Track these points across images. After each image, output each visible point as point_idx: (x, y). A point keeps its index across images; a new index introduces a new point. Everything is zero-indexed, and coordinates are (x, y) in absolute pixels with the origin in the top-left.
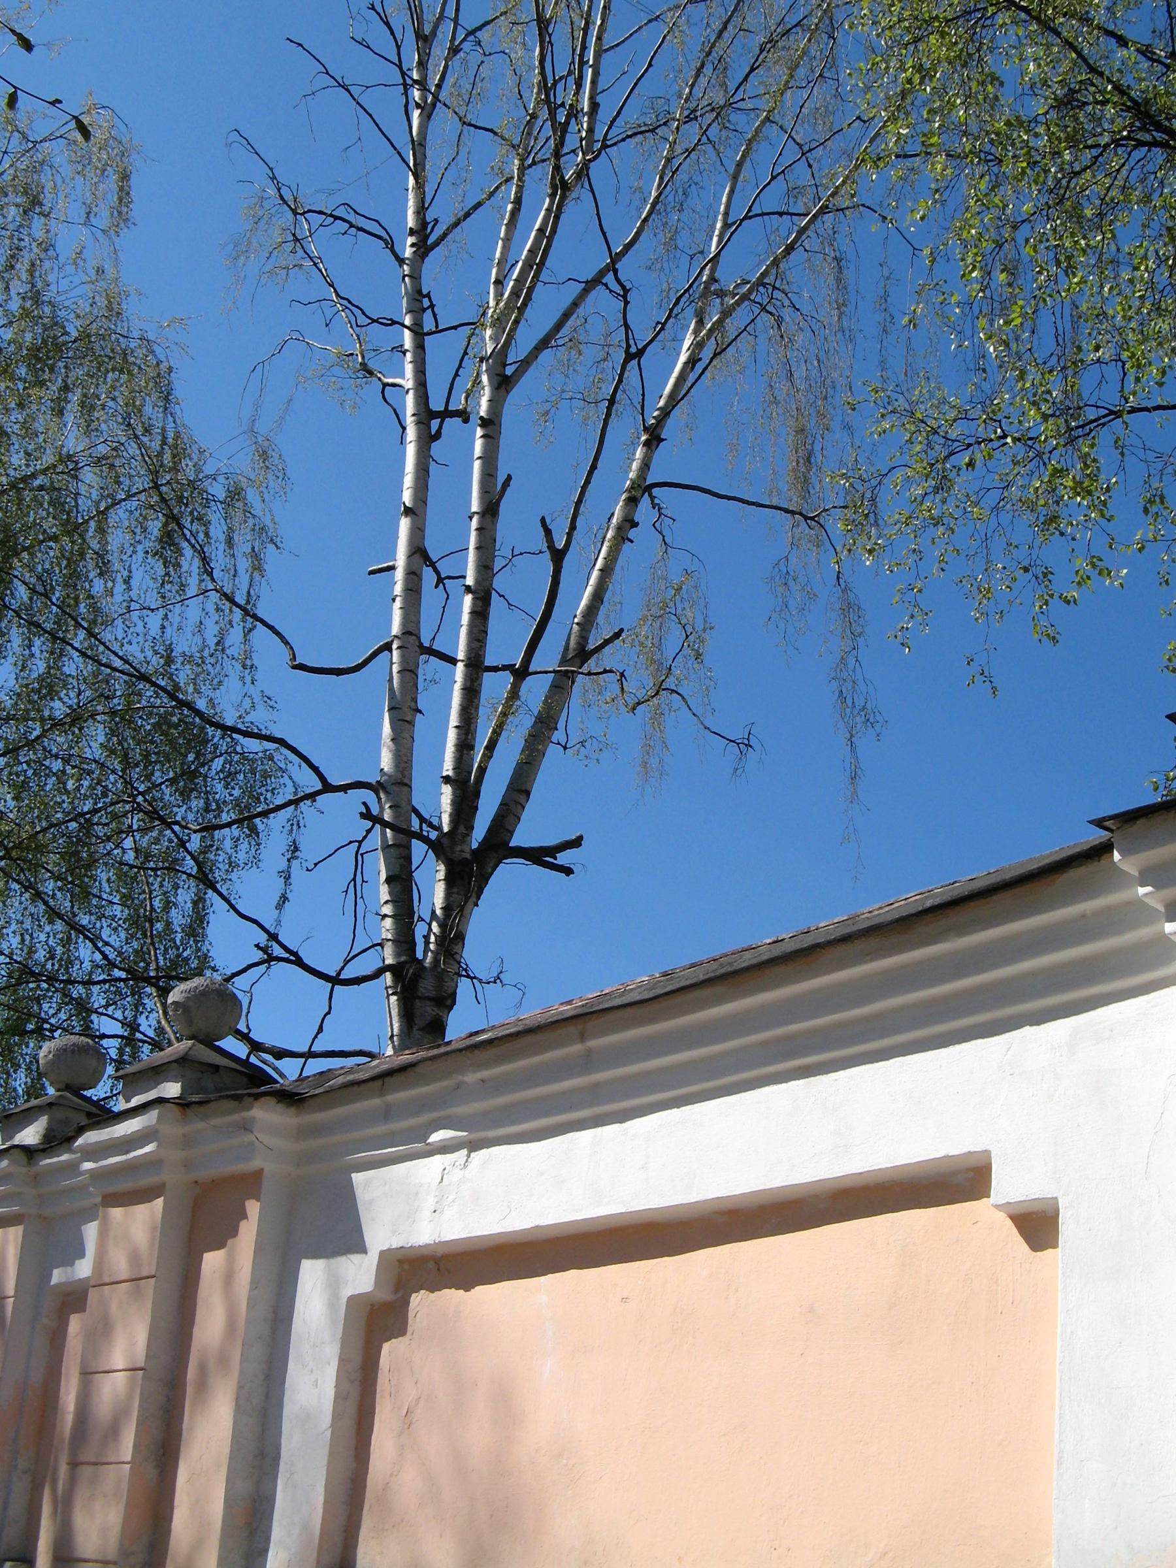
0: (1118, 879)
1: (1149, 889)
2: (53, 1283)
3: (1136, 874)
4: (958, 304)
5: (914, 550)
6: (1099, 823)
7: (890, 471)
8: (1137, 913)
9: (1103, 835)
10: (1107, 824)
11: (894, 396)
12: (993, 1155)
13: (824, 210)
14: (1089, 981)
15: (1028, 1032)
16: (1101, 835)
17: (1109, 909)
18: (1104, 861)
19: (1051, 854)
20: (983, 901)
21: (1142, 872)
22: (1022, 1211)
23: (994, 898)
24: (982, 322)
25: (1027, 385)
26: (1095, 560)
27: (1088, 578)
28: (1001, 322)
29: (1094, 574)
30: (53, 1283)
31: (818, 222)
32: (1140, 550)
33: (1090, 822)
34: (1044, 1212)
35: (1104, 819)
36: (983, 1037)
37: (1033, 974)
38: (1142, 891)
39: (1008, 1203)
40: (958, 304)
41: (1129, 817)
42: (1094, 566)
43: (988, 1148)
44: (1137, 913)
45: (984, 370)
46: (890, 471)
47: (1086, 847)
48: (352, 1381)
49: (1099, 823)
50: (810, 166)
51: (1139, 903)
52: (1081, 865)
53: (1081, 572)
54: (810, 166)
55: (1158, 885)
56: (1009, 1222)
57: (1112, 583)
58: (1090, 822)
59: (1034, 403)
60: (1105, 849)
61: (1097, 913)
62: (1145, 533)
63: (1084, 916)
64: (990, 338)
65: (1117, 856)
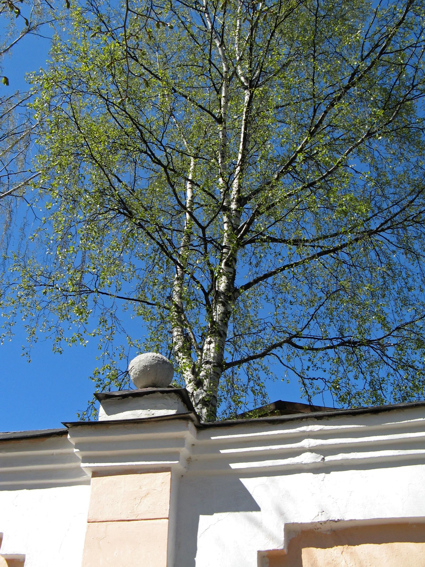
0: (67, 444)
1: (78, 450)
2: (230, 465)
3: (74, 444)
4: (53, 240)
5: (13, 313)
6: (65, 424)
7: (13, 284)
8: (71, 458)
9: (65, 428)
10: (67, 425)
11: (21, 260)
12: (4, 535)
13: (10, 194)
14: (50, 477)
15: (25, 492)
16: (64, 428)
17: (62, 454)
18: (63, 437)
19: (44, 431)
20: (17, 441)
21: (76, 444)
22: (11, 558)
23: (22, 441)
24: (59, 248)
25: (70, 273)
26: (80, 335)
27: (76, 340)
28: (65, 250)
29: (78, 339)
30: (230, 465)
31: (6, 197)
32: (94, 336)
33: (62, 423)
34: (19, 559)
35: (67, 423)
36: (8, 490)
37: (31, 471)
38: (75, 450)
39: (6, 554)
40: (53, 240)
41: (75, 424)
42: (79, 337)
43: (262, 509)
44: (71, 458)
45: (55, 264)
46: (13, 284)
47: (380, 414)
48: (316, 525)
49: (65, 424)
50: (9, 178)
51: (73, 454)
52: (55, 437)
53: (74, 338)
54: (9, 178)
55: (81, 450)
56: (5, 562)
57: (82, 344)
58: (62, 423)
59: (71, 280)
60: (65, 433)
61: (57, 454)
62: (96, 331)
63: (53, 454)
64: (60, 254)
65: (69, 436)
